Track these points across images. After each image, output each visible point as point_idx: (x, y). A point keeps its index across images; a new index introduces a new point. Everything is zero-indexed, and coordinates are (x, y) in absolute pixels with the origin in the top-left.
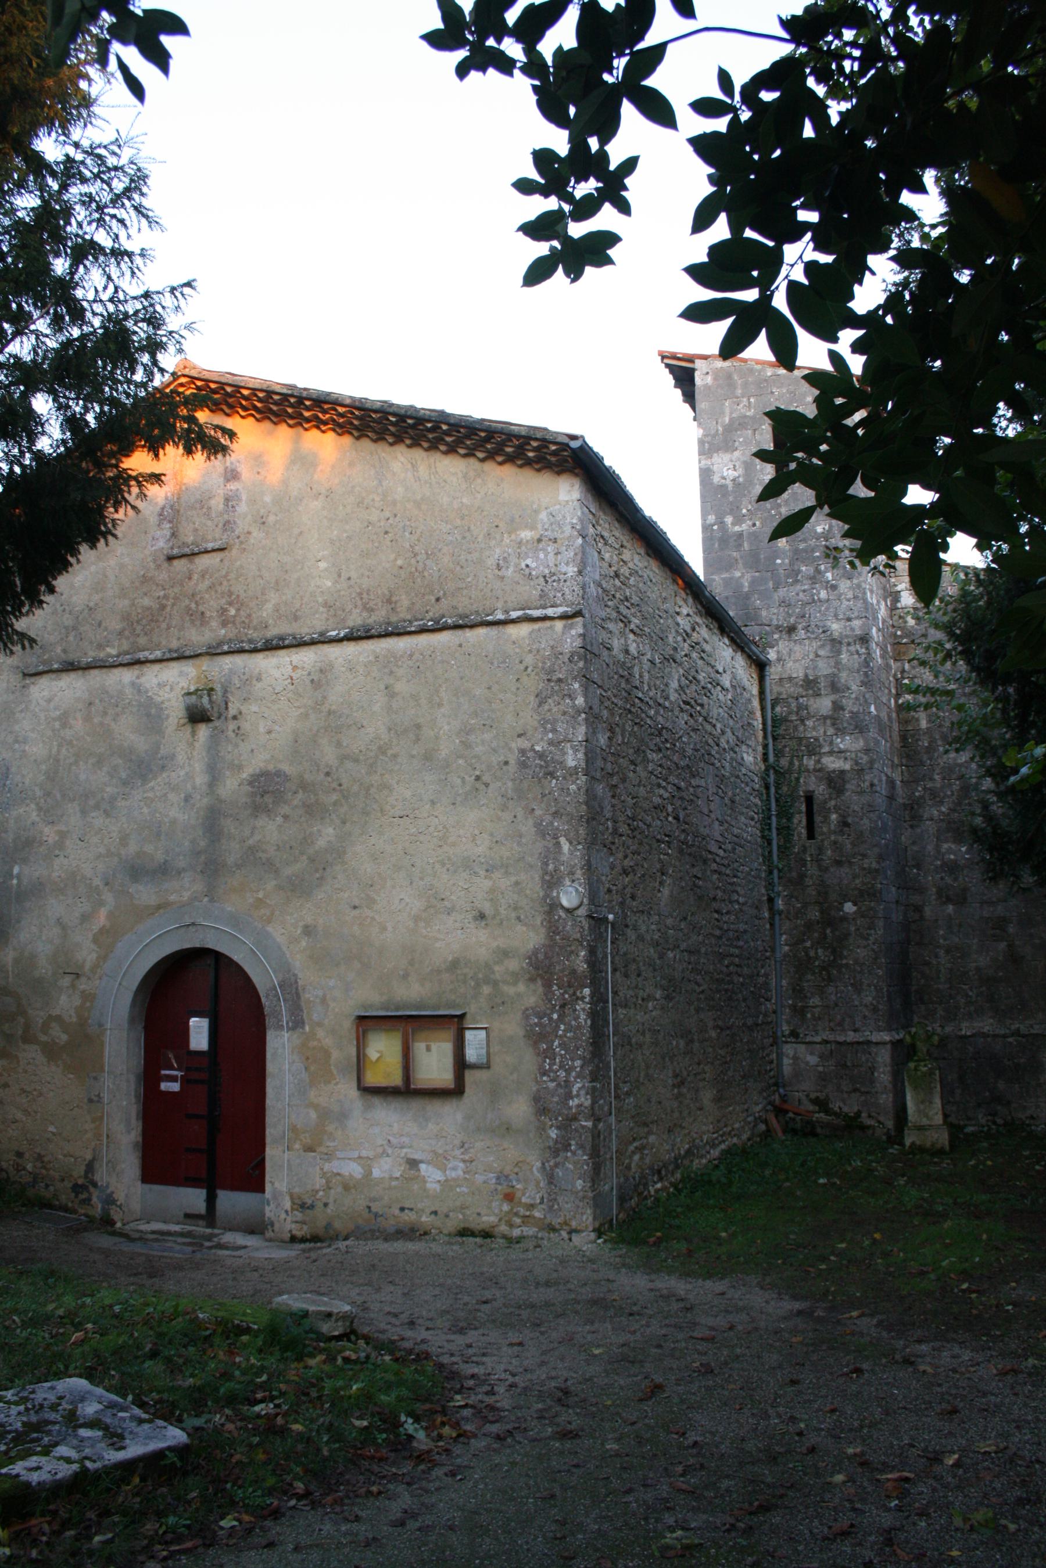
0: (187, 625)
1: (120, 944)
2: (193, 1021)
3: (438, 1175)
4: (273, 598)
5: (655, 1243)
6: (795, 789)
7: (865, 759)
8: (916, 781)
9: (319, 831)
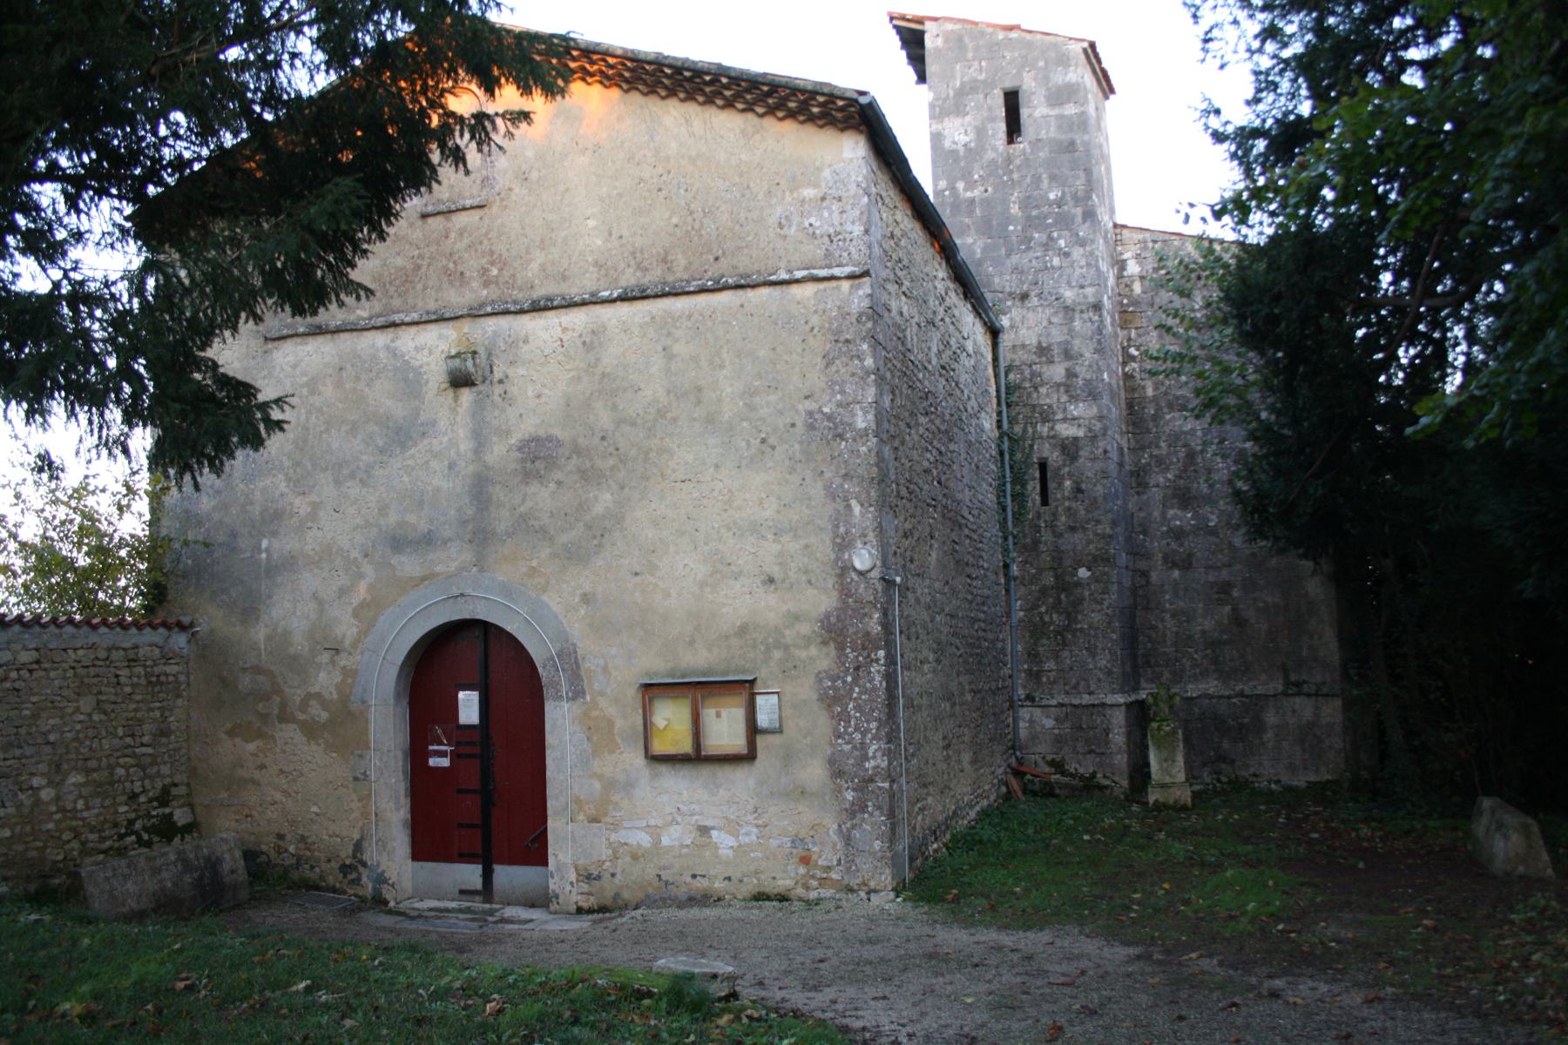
0: (445, 285)
1: (382, 618)
2: (461, 695)
3: (730, 841)
4: (539, 258)
5: (953, 901)
6: (1029, 456)
7: (1098, 426)
8: (1143, 448)
9: (596, 497)
